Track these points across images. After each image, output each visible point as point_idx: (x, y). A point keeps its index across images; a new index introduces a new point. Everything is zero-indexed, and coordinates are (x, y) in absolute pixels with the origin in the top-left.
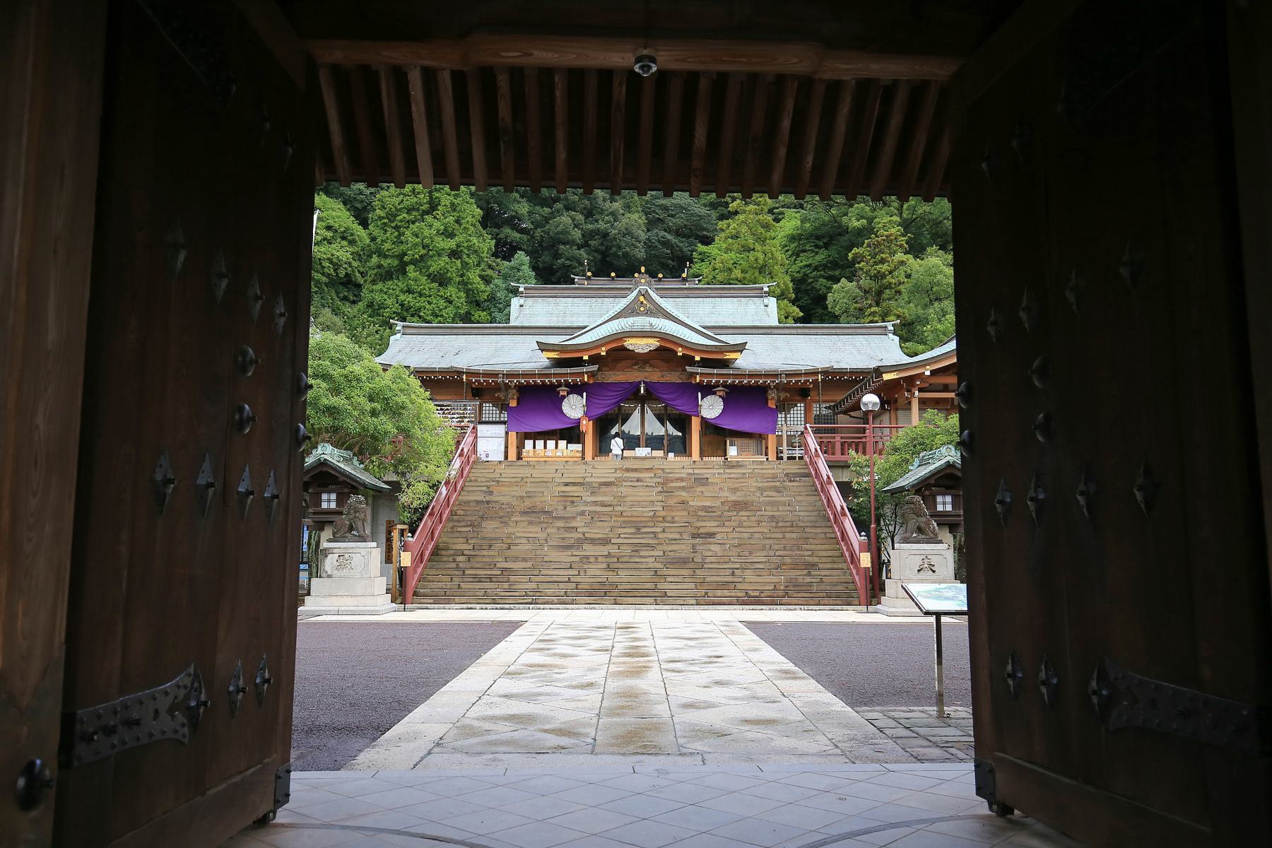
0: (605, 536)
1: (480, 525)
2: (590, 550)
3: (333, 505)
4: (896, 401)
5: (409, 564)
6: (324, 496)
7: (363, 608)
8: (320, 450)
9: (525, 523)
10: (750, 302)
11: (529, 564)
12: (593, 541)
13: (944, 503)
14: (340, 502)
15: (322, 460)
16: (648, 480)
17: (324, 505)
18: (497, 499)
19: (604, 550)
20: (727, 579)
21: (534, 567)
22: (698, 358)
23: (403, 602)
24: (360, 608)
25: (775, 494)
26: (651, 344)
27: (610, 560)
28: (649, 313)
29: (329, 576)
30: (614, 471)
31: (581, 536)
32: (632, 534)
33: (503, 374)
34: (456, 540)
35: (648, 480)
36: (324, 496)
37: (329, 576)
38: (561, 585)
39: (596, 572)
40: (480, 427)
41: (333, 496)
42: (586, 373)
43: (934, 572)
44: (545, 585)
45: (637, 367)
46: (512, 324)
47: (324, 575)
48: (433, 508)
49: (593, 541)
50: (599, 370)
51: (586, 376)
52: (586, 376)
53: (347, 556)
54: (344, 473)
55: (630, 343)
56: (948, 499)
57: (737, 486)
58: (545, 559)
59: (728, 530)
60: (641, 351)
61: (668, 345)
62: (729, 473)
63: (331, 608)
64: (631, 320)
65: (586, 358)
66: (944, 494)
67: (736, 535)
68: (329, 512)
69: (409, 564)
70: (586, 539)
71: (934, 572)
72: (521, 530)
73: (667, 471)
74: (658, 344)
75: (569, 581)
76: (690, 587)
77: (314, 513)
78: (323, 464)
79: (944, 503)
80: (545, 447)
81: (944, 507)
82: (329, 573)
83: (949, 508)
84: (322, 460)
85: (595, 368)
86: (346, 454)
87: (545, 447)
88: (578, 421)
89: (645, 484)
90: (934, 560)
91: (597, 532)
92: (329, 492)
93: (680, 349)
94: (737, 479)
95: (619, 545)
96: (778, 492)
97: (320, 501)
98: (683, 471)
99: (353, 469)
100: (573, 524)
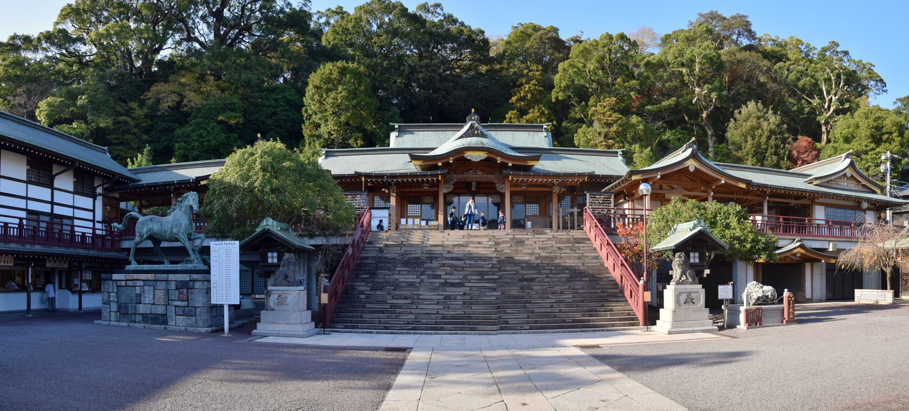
0: (460, 281)
1: (375, 274)
2: (450, 291)
3: (275, 261)
4: (633, 195)
5: (327, 302)
6: (270, 254)
7: (294, 333)
8: (264, 223)
9: (405, 272)
10: (535, 135)
11: (409, 301)
12: (452, 285)
13: (272, 257)
14: (280, 258)
15: (266, 229)
16: (486, 243)
17: (270, 261)
18: (386, 255)
19: (462, 290)
20: (548, 310)
21: (412, 303)
22: (510, 164)
23: (324, 327)
24: (293, 333)
25: (570, 252)
26: (482, 155)
27: (466, 297)
28: (478, 135)
29: (273, 310)
30: (462, 237)
31: (443, 281)
32: (478, 280)
33: (387, 176)
34: (360, 284)
35: (486, 243)
36: (270, 254)
37: (273, 310)
38: (432, 316)
39: (456, 309)
40: (373, 211)
41: (275, 254)
42: (440, 174)
43: (694, 303)
44: (421, 316)
45: (471, 172)
46: (392, 146)
47: (269, 309)
48: (343, 262)
49: (452, 285)
50: (448, 173)
51: (440, 176)
52: (440, 176)
53: (283, 296)
54: (281, 238)
55: (469, 155)
56: (697, 255)
57: (544, 246)
58: (421, 297)
59: (543, 276)
60: (475, 160)
61: (491, 156)
62: (538, 238)
63: (273, 332)
64: (469, 139)
65: (440, 164)
66: (694, 252)
67: (549, 280)
68: (273, 265)
69: (327, 302)
70: (447, 283)
71: (694, 303)
72: (405, 277)
73: (497, 237)
74: (486, 156)
75: (438, 313)
76: (523, 317)
77: (263, 266)
78: (267, 233)
79: (272, 257)
80: (407, 223)
81: (694, 260)
82: (272, 307)
83: (697, 261)
84: (266, 229)
85: (446, 171)
86: (284, 225)
87: (407, 223)
88: (232, 308)
89: (484, 246)
90: (693, 296)
91: (455, 278)
92: (272, 252)
93: (499, 158)
94: (543, 241)
95: (471, 288)
96: (572, 250)
97: (267, 258)
98: (507, 236)
99: (292, 238)
100: (438, 273)
